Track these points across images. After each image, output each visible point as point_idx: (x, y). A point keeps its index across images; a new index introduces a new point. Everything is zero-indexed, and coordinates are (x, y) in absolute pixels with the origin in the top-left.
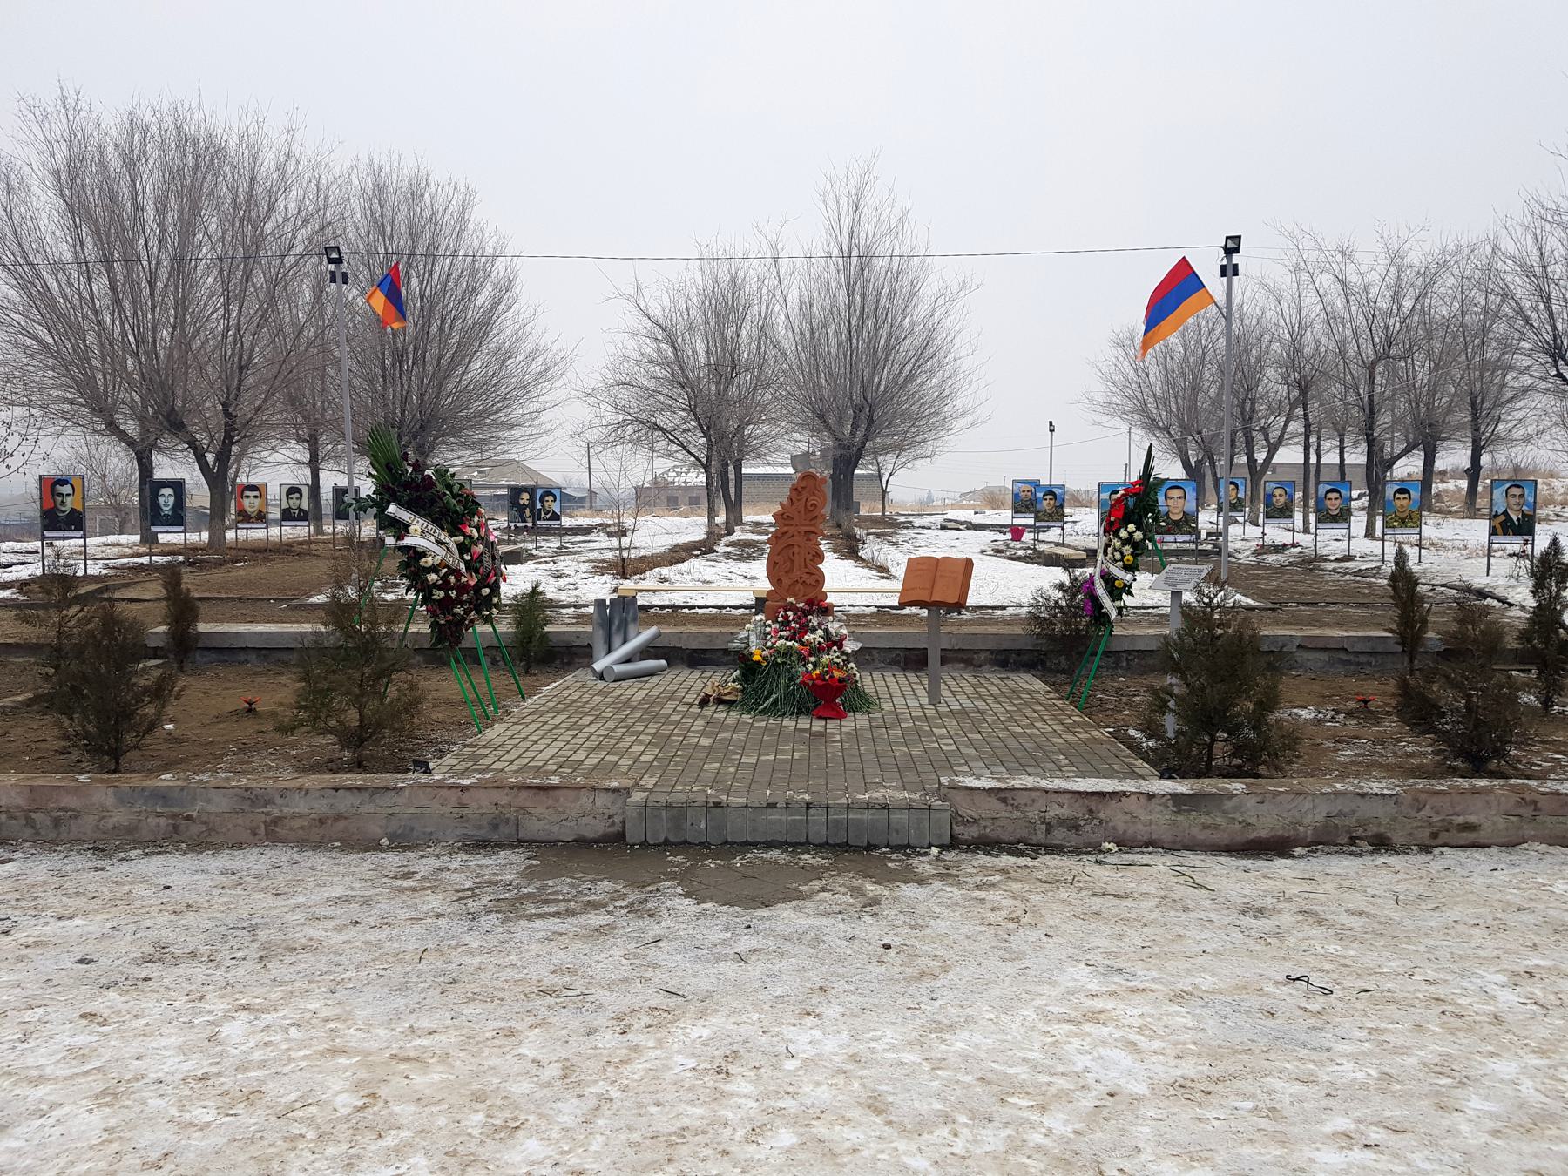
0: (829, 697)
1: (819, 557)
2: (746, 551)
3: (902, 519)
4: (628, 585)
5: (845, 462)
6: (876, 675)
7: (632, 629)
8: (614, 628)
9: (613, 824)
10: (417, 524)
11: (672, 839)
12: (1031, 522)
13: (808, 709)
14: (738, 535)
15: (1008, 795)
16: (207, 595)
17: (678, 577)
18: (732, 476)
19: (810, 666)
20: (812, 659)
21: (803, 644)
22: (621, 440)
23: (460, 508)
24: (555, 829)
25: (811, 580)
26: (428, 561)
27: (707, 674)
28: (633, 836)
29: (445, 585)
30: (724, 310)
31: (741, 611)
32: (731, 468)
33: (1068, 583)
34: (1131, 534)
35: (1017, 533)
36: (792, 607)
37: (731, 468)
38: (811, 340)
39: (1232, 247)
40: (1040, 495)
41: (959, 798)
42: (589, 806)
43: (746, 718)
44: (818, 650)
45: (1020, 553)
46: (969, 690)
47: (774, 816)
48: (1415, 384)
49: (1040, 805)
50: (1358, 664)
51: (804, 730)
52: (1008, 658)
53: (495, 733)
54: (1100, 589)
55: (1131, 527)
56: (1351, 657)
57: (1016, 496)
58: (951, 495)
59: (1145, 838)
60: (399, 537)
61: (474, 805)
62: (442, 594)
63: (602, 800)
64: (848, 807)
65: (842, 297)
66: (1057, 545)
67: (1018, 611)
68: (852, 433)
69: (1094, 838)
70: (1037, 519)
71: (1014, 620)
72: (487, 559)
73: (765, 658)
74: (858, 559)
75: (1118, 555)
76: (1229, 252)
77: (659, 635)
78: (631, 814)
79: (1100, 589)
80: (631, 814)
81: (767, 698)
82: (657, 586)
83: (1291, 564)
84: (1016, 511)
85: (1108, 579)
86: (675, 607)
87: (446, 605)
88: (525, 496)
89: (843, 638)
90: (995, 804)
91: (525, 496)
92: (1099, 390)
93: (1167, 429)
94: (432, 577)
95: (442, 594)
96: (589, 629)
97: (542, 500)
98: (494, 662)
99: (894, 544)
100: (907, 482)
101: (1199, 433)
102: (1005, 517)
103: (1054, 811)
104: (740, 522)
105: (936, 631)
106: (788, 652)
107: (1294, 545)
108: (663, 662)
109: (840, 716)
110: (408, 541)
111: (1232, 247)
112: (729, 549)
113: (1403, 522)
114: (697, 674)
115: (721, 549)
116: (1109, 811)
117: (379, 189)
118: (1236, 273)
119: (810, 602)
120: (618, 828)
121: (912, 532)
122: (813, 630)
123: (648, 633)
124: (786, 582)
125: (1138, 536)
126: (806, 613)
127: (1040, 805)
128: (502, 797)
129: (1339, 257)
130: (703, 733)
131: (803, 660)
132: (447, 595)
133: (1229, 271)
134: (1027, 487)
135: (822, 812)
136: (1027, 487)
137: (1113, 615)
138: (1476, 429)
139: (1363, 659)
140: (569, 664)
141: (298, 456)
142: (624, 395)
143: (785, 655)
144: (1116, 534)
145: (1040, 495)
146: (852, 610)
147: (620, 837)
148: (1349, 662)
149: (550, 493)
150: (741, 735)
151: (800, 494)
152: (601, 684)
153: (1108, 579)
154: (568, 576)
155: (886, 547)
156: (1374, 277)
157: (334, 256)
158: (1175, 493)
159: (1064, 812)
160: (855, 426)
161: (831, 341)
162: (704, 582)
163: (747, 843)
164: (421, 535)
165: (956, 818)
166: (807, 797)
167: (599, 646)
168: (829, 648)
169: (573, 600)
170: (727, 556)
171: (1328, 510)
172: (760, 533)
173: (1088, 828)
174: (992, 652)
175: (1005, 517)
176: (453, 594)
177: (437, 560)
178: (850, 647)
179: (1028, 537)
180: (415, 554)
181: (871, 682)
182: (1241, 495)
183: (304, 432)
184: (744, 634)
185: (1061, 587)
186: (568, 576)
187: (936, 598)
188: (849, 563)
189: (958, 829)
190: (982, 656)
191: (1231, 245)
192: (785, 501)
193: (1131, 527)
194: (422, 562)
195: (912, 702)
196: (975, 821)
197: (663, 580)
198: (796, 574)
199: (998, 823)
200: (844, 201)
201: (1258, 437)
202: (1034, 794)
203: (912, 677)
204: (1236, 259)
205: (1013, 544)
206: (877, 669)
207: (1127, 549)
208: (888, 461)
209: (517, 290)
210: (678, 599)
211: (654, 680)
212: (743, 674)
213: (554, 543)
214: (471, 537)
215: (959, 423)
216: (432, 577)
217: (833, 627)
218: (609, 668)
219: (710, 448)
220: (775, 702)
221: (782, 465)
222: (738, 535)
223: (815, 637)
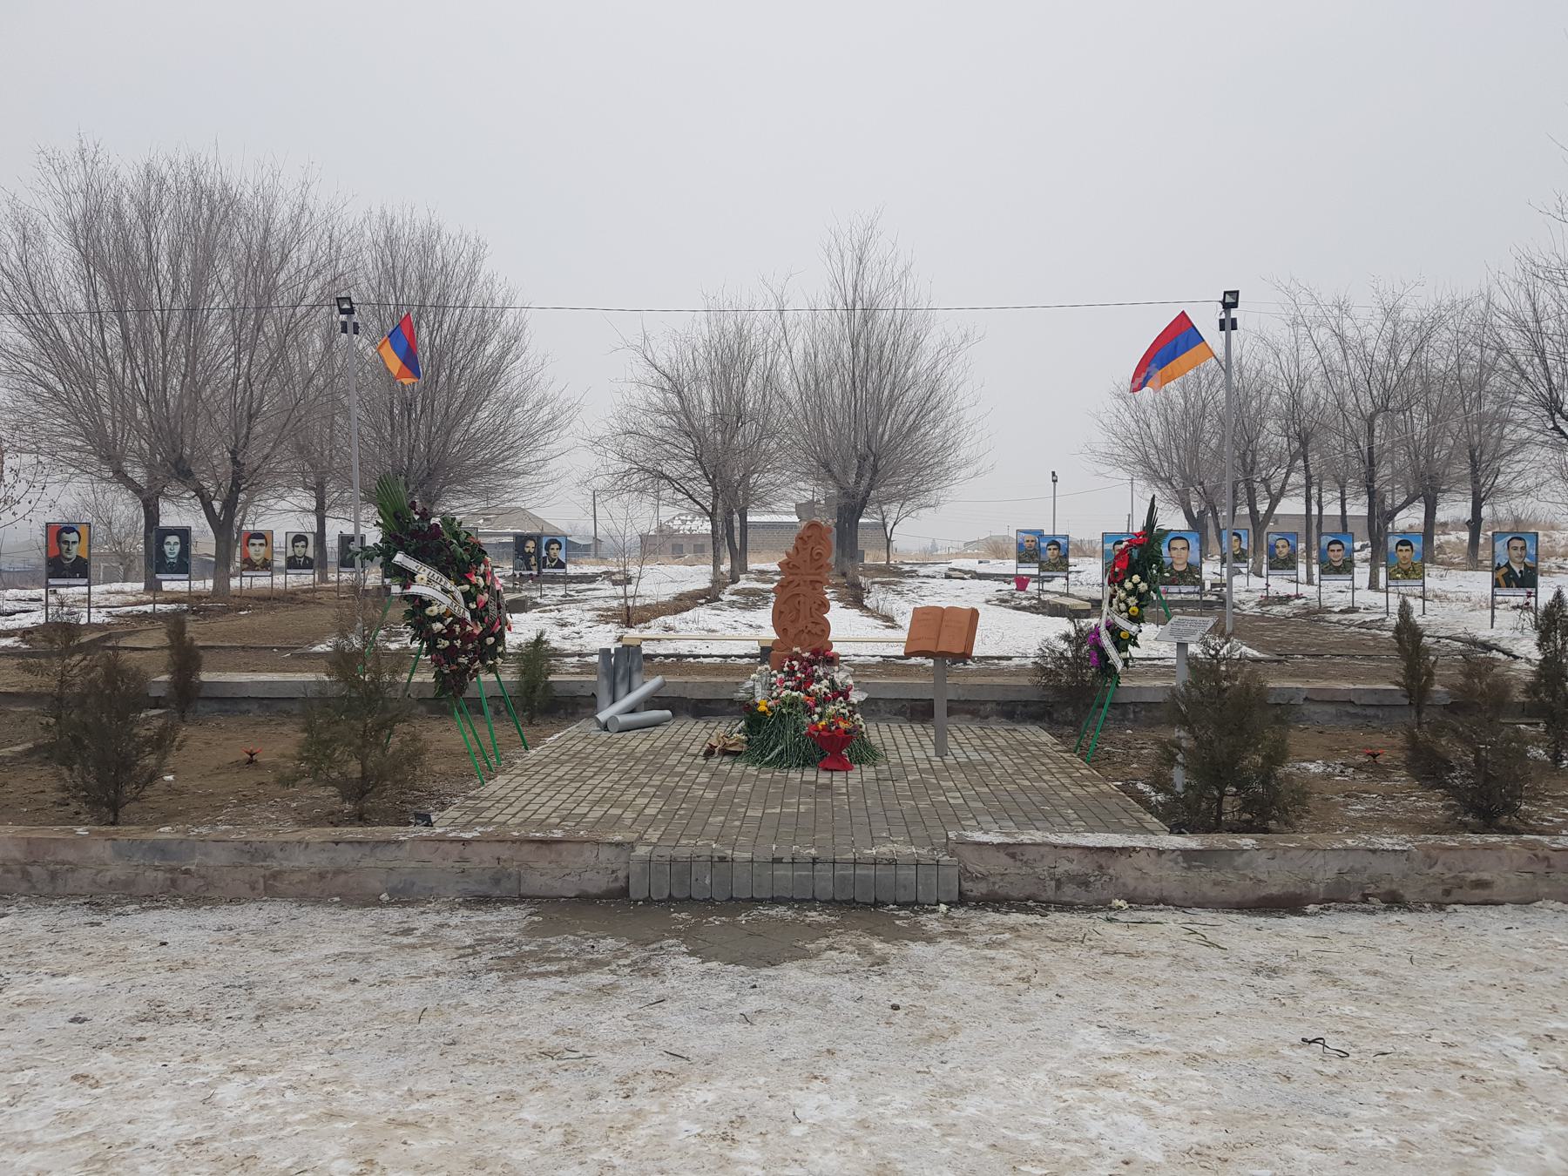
0: (835, 749)
1: (825, 606)
2: (751, 600)
3: (907, 568)
4: (633, 633)
5: (850, 510)
6: (883, 726)
7: (636, 678)
8: (619, 678)
9: (616, 879)
10: (424, 572)
11: (675, 894)
12: (1035, 571)
13: (813, 761)
14: (743, 584)
15: (1018, 850)
16: (210, 643)
17: (683, 626)
18: (737, 524)
19: (816, 717)
20: (818, 710)
21: (808, 694)
22: (627, 489)
23: (466, 557)
24: (557, 884)
25: (817, 630)
26: (433, 610)
27: (712, 725)
28: (637, 891)
29: (449, 634)
30: (730, 362)
31: (746, 660)
32: (736, 516)
33: (1073, 634)
34: (1135, 585)
35: (1022, 582)
36: (797, 657)
37: (736, 516)
38: (815, 391)
39: (1230, 301)
40: (1044, 545)
41: (967, 853)
42: (592, 861)
43: (752, 770)
44: (824, 701)
45: (1025, 603)
46: (976, 742)
47: (780, 871)
48: (1415, 437)
49: (1049, 861)
50: (1366, 717)
51: (810, 783)
52: (1014, 710)
53: (497, 785)
54: (1106, 641)
55: (1136, 578)
56: (1358, 710)
57: (1020, 546)
58: (955, 544)
59: (1156, 895)
60: (405, 586)
61: (476, 860)
62: (447, 643)
63: (606, 854)
64: (855, 862)
65: (846, 348)
66: (1061, 594)
67: (1024, 661)
68: (857, 483)
69: (1105, 895)
70: (1041, 568)
71: (1020, 671)
72: (492, 607)
73: (770, 709)
74: (863, 608)
75: (1123, 606)
76: (1227, 306)
77: (664, 684)
78: (635, 868)
79: (1106, 641)
80: (635, 868)
81: (772, 750)
82: (662, 635)
83: (1295, 615)
84: (1021, 560)
85: (1114, 630)
86: (680, 657)
87: (451, 654)
88: (531, 544)
89: (849, 688)
90: (1003, 859)
91: (531, 544)
92: (1101, 441)
93: (1169, 480)
94: (438, 626)
95: (447, 643)
96: (593, 678)
97: (547, 548)
98: (497, 712)
99: (899, 593)
100: (911, 531)
101: (1201, 483)
102: (1010, 566)
103: (1064, 867)
104: (745, 571)
105: (941, 682)
106: (793, 703)
107: (1298, 597)
108: (668, 712)
109: (846, 768)
110: (414, 589)
111: (1230, 301)
112: (734, 598)
113: (1406, 574)
114: (701, 724)
115: (726, 597)
116: (1118, 867)
117: (391, 241)
118: (1234, 327)
119: (815, 652)
120: (621, 883)
121: (916, 582)
122: (819, 680)
123: (653, 683)
124: (792, 631)
125: (1143, 587)
126: (811, 663)
127: (1049, 861)
128: (505, 852)
129: (1336, 311)
130: (707, 785)
131: (809, 711)
132: (452, 646)
133: (1228, 325)
134: (1031, 537)
135: (829, 867)
136: (1031, 537)
137: (1120, 666)
138: (1476, 481)
139: (1371, 712)
140: (573, 714)
141: (304, 504)
142: (630, 443)
143: (791, 705)
144: (1121, 585)
145: (1044, 545)
146: (858, 660)
147: (624, 892)
148: (1356, 715)
149: (555, 541)
150: (746, 788)
151: (805, 543)
152: (605, 735)
153: (1114, 630)
154: (573, 624)
155: (890, 596)
156: (1371, 331)
157: (346, 306)
158: (1179, 544)
159: (1073, 868)
160: (860, 476)
161: (835, 390)
162: (710, 631)
163: (752, 899)
164: (428, 584)
165: (964, 874)
166: (813, 851)
167: (603, 696)
168: (835, 698)
169: (577, 648)
170: (732, 604)
171: (1330, 561)
172: (765, 582)
173: (1098, 884)
174: (998, 703)
175: (1010, 566)
176: (458, 643)
177: (443, 609)
178: (856, 697)
179: (1032, 587)
180: (422, 603)
181: (877, 733)
182: (1244, 546)
183: (311, 480)
184: (749, 684)
185: (1066, 637)
186: (573, 624)
187: (943, 648)
188: (855, 612)
189: (967, 885)
190: (989, 707)
191: (1229, 299)
192: (791, 550)
193: (1136, 578)
194: (428, 611)
195: (919, 754)
196: (984, 878)
197: (668, 629)
198: (801, 624)
199: (1007, 879)
200: (848, 255)
201: (1260, 488)
202: (1043, 850)
203: (918, 728)
204: (1234, 313)
205: (1018, 594)
206: (882, 720)
207: (1132, 601)
208: (893, 510)
209: (526, 338)
210: (683, 647)
211: (659, 731)
212: (748, 725)
213: (559, 591)
214: (477, 586)
215: (963, 473)
216: (438, 626)
217: (840, 677)
218: (613, 718)
219: (716, 497)
220: (781, 753)
221: (787, 513)
222: (743, 584)
223: (820, 687)
